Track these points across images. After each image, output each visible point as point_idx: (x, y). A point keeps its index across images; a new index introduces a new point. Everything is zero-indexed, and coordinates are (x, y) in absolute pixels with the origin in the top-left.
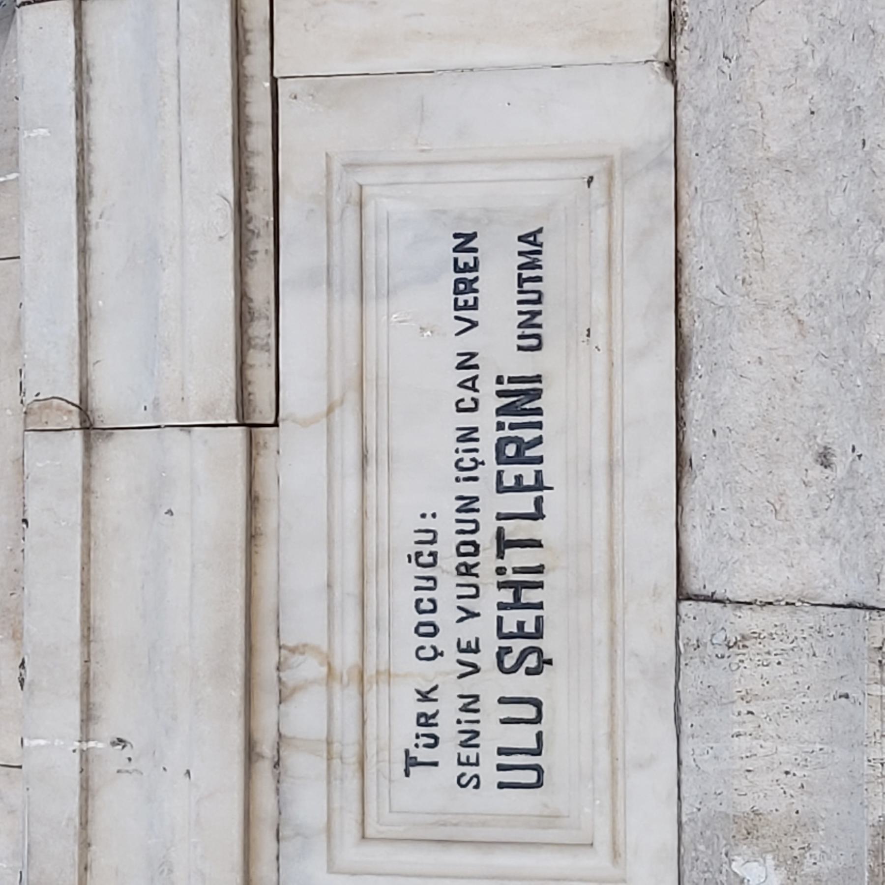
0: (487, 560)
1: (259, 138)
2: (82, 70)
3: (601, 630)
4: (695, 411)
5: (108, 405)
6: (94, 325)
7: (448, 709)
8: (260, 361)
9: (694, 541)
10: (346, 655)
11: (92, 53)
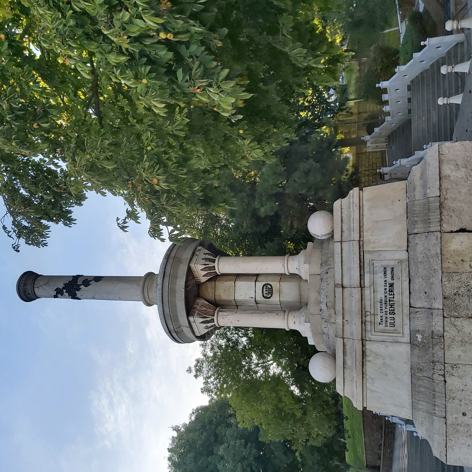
0: (388, 303)
1: (362, 257)
2: (342, 249)
3: (401, 310)
4: (411, 287)
5: (345, 284)
6: (343, 276)
7: (384, 318)
8: (362, 281)
9: (411, 301)
10: (373, 312)
11: (343, 248)
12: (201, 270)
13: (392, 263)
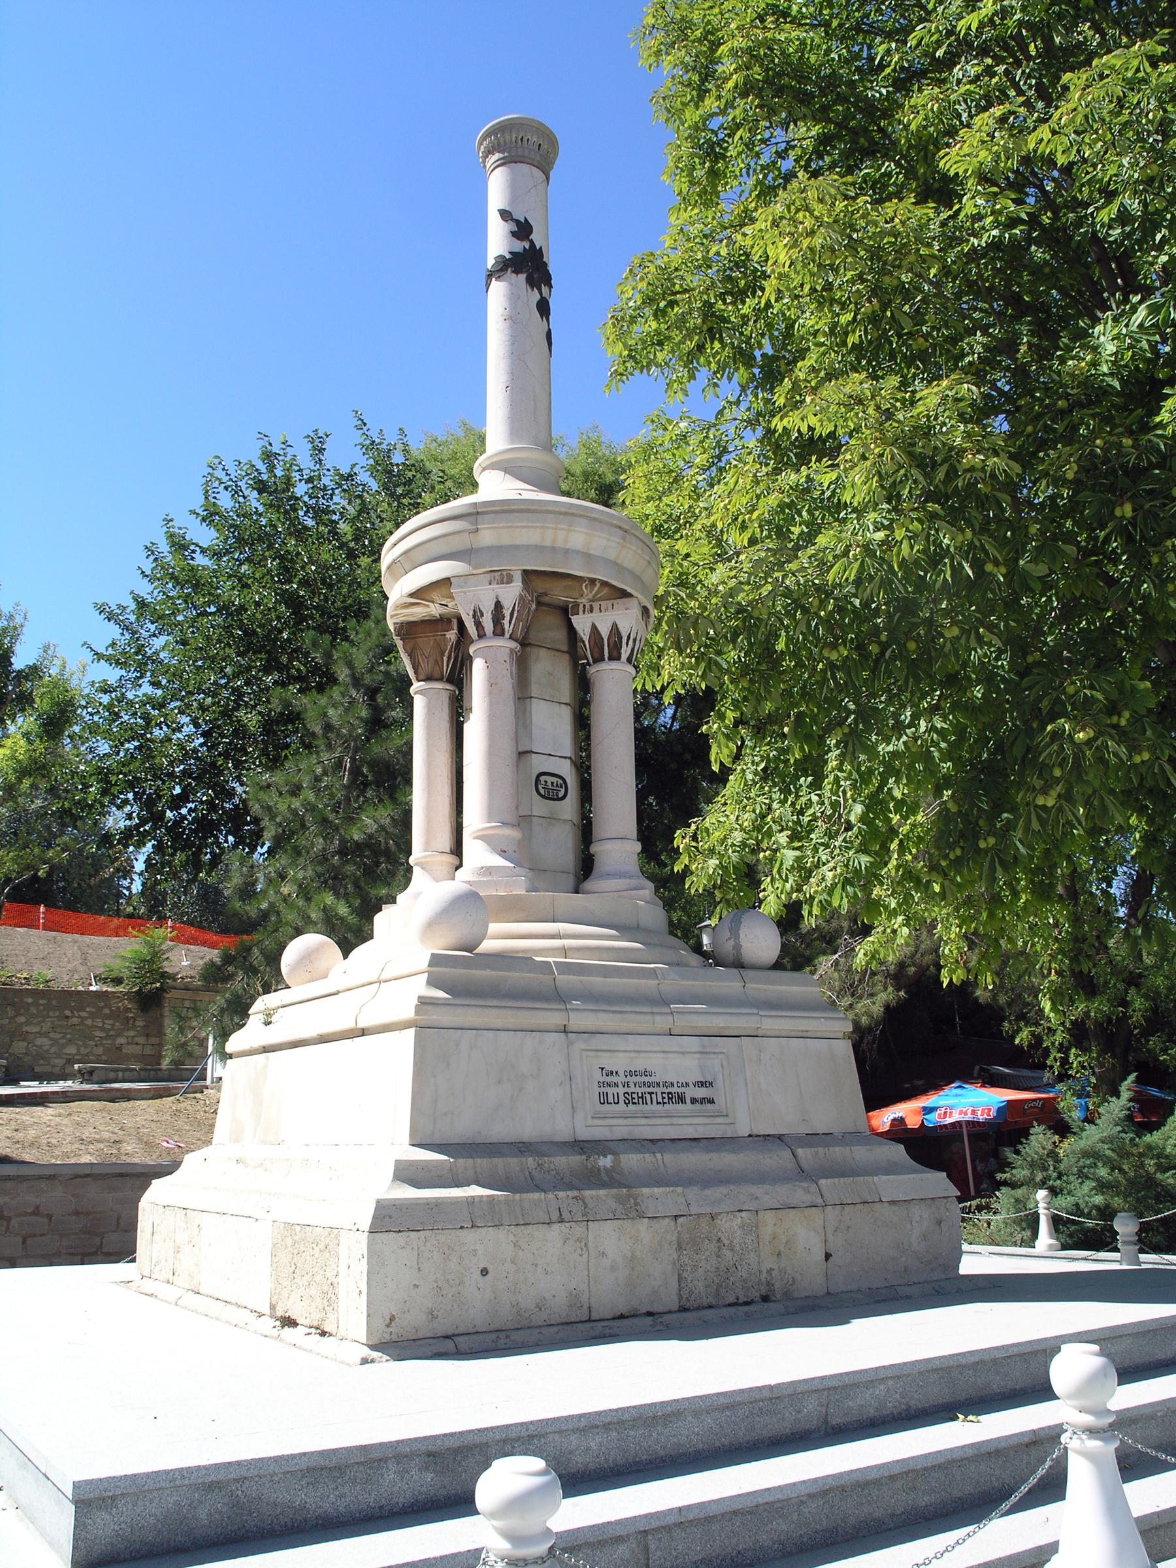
12: (594, 626)
13: (720, 1101)
